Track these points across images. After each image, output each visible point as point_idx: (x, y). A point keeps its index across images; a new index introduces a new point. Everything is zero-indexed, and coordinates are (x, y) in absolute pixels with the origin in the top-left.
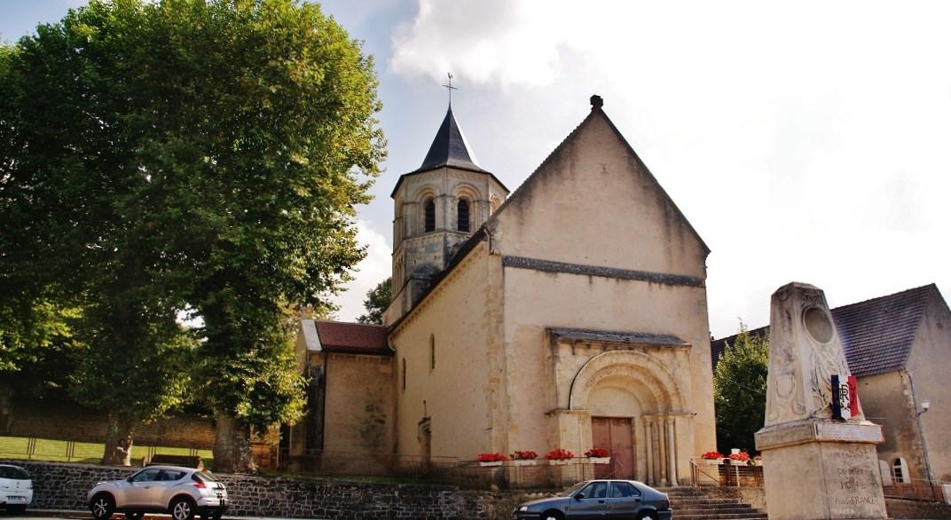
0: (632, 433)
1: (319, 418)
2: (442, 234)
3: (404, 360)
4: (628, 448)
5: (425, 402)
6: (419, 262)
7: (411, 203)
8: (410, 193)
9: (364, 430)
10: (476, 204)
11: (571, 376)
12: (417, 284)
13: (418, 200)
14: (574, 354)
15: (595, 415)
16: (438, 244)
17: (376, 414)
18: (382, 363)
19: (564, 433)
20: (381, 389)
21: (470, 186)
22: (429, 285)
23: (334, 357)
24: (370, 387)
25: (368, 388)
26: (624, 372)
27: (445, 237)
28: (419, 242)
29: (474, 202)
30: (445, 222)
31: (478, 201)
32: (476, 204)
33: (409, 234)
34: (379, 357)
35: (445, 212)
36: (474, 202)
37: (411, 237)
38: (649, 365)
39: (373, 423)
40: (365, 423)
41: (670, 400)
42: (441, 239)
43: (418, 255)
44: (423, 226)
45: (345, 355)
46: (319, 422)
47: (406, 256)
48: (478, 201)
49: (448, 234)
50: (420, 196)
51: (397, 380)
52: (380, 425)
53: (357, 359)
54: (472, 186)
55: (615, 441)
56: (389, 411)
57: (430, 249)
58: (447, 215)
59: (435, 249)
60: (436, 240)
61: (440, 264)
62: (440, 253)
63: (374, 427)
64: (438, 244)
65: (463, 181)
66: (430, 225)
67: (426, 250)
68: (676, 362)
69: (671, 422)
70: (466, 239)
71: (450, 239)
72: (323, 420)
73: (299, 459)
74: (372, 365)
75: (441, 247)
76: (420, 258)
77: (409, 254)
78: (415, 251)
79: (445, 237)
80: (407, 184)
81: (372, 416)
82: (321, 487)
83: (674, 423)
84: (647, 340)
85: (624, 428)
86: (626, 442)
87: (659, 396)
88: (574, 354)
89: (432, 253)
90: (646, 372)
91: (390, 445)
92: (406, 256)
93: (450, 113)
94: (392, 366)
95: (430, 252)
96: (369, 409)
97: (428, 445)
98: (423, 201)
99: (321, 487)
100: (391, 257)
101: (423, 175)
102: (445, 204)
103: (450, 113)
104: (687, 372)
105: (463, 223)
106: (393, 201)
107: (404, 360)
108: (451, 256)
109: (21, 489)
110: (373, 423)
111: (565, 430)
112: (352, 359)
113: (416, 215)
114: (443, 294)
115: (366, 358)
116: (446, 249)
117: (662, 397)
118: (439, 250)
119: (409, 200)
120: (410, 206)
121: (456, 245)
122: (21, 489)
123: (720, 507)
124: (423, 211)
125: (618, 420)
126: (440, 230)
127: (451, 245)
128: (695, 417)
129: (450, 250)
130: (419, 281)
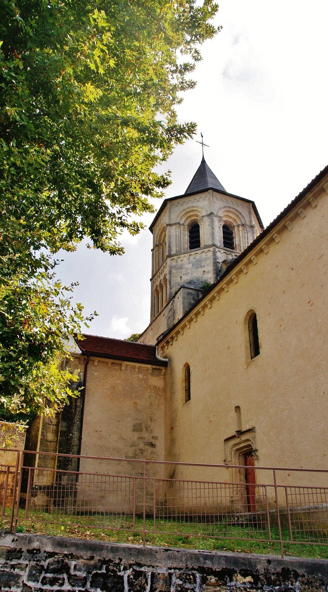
1: (76, 434)
2: (211, 249)
3: (187, 369)
5: (238, 408)
6: (186, 278)
7: (175, 224)
8: (175, 214)
9: (130, 454)
10: (241, 228)
12: (188, 293)
13: (182, 222)
16: (206, 259)
17: (146, 435)
18: (152, 374)
20: (151, 404)
21: (234, 211)
22: (201, 296)
23: (96, 363)
24: (138, 401)
25: (136, 403)
27: (214, 253)
28: (185, 259)
29: (238, 226)
30: (213, 239)
31: (243, 225)
32: (241, 228)
33: (173, 252)
34: (150, 366)
35: (213, 229)
36: (238, 226)
37: (176, 255)
39: (141, 446)
40: (133, 445)
42: (210, 254)
43: (184, 271)
44: (187, 245)
45: (110, 361)
46: (75, 441)
47: (170, 273)
48: (243, 225)
49: (217, 250)
50: (184, 218)
51: (172, 393)
52: (150, 449)
53: (123, 368)
54: (236, 210)
56: (159, 431)
57: (198, 264)
58: (211, 233)
59: (203, 264)
60: (203, 255)
61: (210, 278)
62: (210, 268)
63: (142, 451)
64: (206, 259)
65: (227, 205)
66: (195, 242)
67: (193, 265)
70: (234, 257)
71: (218, 254)
72: (80, 439)
73: (47, 490)
74: (141, 376)
75: (210, 262)
76: (187, 274)
77: (174, 271)
78: (181, 267)
79: (214, 253)
80: (170, 208)
81: (140, 438)
82: (138, 574)
89: (199, 267)
91: (162, 472)
92: (170, 273)
93: (203, 162)
94: (165, 379)
95: (197, 268)
96: (137, 428)
97: (249, 476)
98: (187, 224)
99: (138, 574)
100: (150, 283)
101: (187, 199)
102: (212, 222)
103: (203, 162)
105: (228, 240)
106: (151, 235)
107: (187, 369)
108: (220, 271)
110: (141, 446)
112: (117, 367)
113: (178, 237)
114: (174, 343)
115: (134, 368)
116: (215, 263)
118: (208, 265)
119: (172, 222)
120: (174, 227)
121: (224, 262)
124: (187, 233)
126: (206, 247)
127: (220, 260)
129: (220, 265)
130: (190, 291)
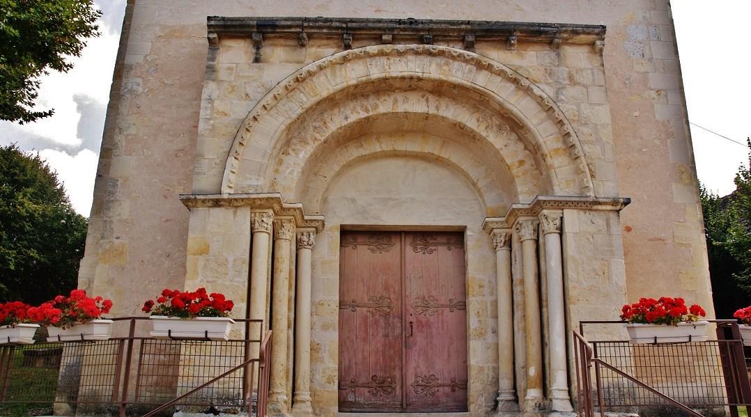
0: (463, 266)
4: (452, 307)
11: (239, 109)
14: (257, 60)
15: (349, 221)
19: (201, 260)
26: (416, 105)
38: (482, 80)
41: (548, 168)
55: (414, 289)
68: (563, 72)
69: (550, 226)
83: (561, 231)
84: (463, 26)
85: (442, 256)
86: (448, 293)
87: (521, 163)
88: (257, 60)
90: (477, 100)
104: (597, 95)
109: (742, 409)
111: (204, 251)
117: (528, 164)
122: (742, 409)
123: (445, 36)
125: (424, 236)
128: (625, 210)
